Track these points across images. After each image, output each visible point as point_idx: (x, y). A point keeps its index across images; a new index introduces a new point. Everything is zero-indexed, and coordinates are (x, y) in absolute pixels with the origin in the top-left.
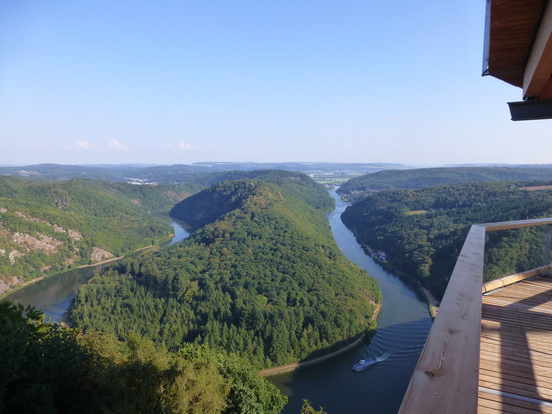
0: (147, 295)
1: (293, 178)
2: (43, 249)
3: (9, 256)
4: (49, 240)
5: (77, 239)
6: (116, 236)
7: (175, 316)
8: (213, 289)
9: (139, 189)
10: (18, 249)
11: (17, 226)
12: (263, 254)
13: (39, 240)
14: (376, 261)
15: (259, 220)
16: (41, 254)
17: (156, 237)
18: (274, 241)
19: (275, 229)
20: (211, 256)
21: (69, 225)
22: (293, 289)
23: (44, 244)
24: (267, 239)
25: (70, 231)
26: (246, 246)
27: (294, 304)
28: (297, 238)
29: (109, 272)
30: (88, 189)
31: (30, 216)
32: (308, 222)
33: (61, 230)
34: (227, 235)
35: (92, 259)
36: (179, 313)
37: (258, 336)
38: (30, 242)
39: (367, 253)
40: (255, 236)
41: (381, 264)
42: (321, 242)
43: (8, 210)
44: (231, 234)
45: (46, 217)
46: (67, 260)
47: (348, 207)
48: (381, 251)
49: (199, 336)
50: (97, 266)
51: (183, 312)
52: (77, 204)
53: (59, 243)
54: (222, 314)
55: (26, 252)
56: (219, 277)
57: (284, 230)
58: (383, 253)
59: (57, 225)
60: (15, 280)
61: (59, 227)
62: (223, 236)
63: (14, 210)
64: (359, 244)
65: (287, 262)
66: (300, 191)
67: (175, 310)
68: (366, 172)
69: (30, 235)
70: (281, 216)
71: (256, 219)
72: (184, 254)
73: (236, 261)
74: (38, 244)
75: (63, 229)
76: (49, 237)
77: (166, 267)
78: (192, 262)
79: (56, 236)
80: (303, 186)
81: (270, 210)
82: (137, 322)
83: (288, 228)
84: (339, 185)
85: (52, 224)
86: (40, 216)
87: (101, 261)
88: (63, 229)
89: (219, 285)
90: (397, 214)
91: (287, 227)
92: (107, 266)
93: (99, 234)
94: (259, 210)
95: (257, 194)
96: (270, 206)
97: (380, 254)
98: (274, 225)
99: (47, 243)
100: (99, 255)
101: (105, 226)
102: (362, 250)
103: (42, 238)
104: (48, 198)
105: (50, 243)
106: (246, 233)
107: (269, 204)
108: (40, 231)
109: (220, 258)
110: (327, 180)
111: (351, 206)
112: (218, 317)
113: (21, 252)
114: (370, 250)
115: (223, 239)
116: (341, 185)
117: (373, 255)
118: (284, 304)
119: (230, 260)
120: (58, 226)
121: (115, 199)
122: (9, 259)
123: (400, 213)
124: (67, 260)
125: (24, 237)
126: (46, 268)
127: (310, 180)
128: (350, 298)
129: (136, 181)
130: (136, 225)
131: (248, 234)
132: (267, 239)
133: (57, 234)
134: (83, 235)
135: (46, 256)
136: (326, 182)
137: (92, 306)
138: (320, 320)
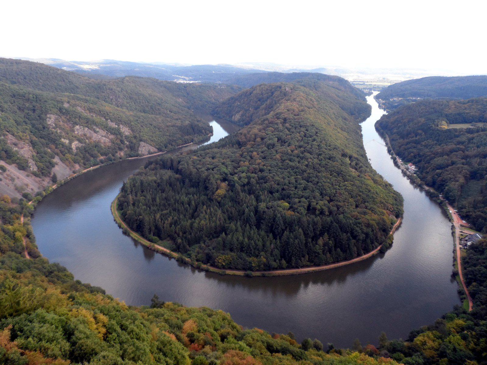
0: (183, 191)
1: (331, 83)
2: (99, 142)
3: (71, 146)
4: (104, 133)
5: (127, 133)
6: (161, 133)
7: (204, 212)
8: (240, 190)
9: (183, 88)
10: (79, 141)
11: (77, 119)
12: (290, 161)
13: (96, 133)
14: (404, 174)
15: (290, 127)
16: (97, 145)
17: (196, 135)
18: (302, 149)
19: (305, 136)
20: (242, 159)
21: (119, 121)
22: (314, 198)
23: (100, 137)
24: (295, 146)
25: (121, 126)
26: (275, 152)
27: (314, 213)
28: (325, 147)
29: (153, 166)
30: (138, 87)
31: (88, 112)
32: (339, 130)
33: (113, 125)
34: (258, 139)
35: (140, 152)
36: (209, 210)
37: (276, 239)
38: (88, 135)
39: (396, 164)
40: (285, 143)
41: (410, 177)
42: (349, 152)
43: (70, 105)
44: (262, 139)
45: (102, 112)
46: (119, 152)
47: (384, 115)
48: (411, 164)
49: (224, 233)
50: (144, 158)
51: (212, 209)
52: (128, 101)
53: (112, 137)
54: (245, 215)
55: (85, 143)
56: (246, 180)
57: (313, 138)
58: (413, 167)
59: (111, 120)
60: (77, 167)
61: (112, 122)
62: (254, 140)
63: (76, 105)
64: (390, 154)
65: (312, 171)
66: (336, 97)
67: (205, 207)
68: (409, 77)
69: (88, 128)
70: (312, 124)
71: (287, 125)
72: (218, 155)
73: (264, 165)
74: (96, 137)
75: (116, 125)
76: (104, 131)
77: (200, 166)
78: (223, 164)
79: (110, 130)
80: (340, 92)
81: (301, 117)
82: (173, 214)
83: (317, 136)
84: (379, 91)
85: (107, 120)
86: (96, 112)
87: (147, 155)
88: (116, 125)
89: (246, 188)
90: (434, 127)
91: (316, 136)
92: (152, 160)
93: (146, 130)
94: (291, 116)
95: (292, 99)
96: (302, 113)
97: (409, 167)
98: (304, 132)
99: (102, 136)
100: (145, 149)
101: (151, 123)
102: (392, 162)
103: (98, 132)
104: (104, 94)
105: (105, 137)
106: (276, 139)
107: (302, 111)
108: (97, 126)
109: (250, 161)
110: (366, 85)
111: (387, 114)
112: (242, 218)
113: (81, 143)
114: (399, 161)
115: (254, 143)
116: (381, 91)
117: (403, 167)
118: (304, 211)
119: (259, 164)
120: (112, 121)
121: (162, 97)
122: (71, 149)
123: (437, 126)
124: (119, 152)
125: (84, 129)
126: (102, 158)
127: (348, 85)
128: (370, 212)
129: (183, 78)
130: (179, 123)
131: (278, 140)
132: (295, 146)
133: (110, 128)
134: (133, 131)
135: (102, 149)
136: (365, 87)
137: (136, 196)
138: (336, 230)
